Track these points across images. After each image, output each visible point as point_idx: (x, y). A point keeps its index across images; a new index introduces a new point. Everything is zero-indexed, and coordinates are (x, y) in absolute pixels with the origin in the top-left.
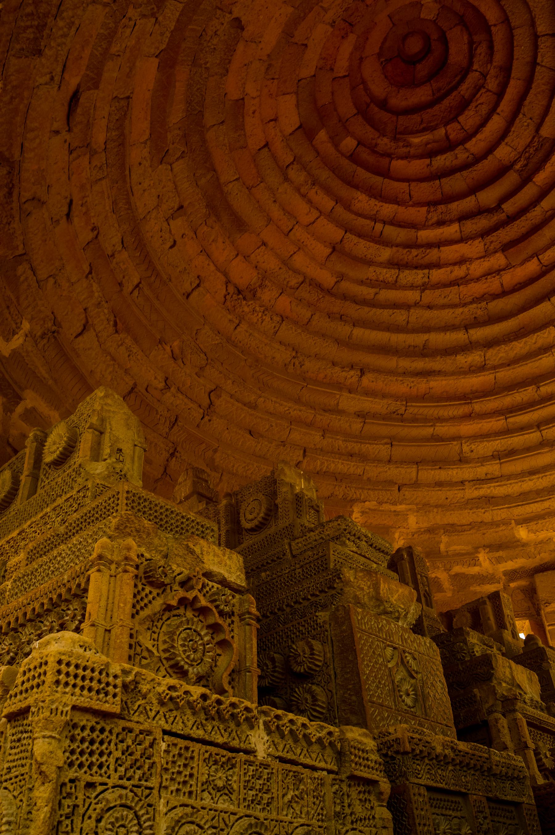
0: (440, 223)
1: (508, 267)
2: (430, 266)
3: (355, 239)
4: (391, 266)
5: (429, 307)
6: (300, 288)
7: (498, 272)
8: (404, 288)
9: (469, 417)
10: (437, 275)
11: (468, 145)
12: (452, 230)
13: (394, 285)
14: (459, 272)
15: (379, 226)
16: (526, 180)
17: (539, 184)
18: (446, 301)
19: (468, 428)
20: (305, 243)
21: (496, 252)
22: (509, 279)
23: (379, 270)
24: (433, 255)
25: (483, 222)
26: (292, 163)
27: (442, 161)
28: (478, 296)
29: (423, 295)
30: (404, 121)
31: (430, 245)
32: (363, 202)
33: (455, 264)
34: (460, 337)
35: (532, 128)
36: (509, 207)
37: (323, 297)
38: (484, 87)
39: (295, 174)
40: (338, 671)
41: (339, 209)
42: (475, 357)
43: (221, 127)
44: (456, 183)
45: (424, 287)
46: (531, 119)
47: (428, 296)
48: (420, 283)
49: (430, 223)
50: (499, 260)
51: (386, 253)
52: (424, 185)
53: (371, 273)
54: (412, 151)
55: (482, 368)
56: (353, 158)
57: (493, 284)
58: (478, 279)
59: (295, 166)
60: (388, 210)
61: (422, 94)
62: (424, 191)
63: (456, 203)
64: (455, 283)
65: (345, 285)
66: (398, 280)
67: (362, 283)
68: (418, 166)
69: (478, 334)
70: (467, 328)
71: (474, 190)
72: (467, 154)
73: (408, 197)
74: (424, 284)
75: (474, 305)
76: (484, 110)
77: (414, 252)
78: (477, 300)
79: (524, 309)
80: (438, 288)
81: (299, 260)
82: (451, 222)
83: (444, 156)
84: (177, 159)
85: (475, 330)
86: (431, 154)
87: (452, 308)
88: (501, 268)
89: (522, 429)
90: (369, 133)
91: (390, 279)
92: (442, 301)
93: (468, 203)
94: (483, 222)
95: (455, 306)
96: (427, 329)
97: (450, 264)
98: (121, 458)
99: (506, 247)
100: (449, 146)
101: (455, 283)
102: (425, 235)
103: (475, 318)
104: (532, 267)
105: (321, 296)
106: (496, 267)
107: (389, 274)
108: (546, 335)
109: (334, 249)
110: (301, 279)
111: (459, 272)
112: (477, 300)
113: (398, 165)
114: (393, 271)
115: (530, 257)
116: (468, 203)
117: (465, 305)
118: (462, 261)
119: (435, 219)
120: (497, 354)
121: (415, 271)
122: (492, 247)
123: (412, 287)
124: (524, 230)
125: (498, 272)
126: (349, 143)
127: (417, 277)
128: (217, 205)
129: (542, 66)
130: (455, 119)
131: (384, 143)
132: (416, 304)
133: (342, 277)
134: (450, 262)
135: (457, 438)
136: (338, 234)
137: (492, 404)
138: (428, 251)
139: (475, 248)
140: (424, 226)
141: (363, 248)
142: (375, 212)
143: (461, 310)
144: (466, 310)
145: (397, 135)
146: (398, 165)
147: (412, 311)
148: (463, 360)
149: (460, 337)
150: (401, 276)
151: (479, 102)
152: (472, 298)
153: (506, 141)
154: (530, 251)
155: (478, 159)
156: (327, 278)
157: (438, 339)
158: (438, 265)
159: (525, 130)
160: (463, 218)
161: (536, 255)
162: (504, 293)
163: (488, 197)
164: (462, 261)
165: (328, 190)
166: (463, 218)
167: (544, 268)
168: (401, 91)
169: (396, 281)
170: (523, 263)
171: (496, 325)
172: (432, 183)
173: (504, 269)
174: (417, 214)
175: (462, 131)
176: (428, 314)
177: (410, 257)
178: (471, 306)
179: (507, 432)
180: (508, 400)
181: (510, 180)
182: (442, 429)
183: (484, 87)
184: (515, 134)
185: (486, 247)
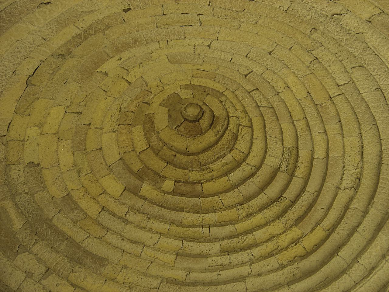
0: (249, 216)
2: (250, 247)
3: (191, 244)
4: (223, 254)
5: (259, 275)
6: (161, 287)
8: (236, 266)
10: (257, 252)
11: (248, 161)
12: (259, 218)
13: (229, 266)
14: (270, 246)
15: (206, 230)
16: (292, 175)
17: (301, 176)
18: (269, 268)
20: (155, 257)
21: (292, 226)
23: (214, 259)
24: (249, 239)
25: (275, 209)
26: (128, 212)
27: (235, 176)
28: (291, 259)
29: (252, 267)
30: (203, 157)
31: (246, 232)
32: (189, 217)
33: (266, 241)
35: (279, 143)
36: (289, 195)
37: (179, 288)
38: (241, 125)
39: (132, 217)
41: (174, 228)
43: (60, 215)
44: (249, 188)
45: (251, 262)
46: (276, 138)
47: (256, 268)
48: (247, 260)
49: (242, 217)
51: (216, 247)
52: (229, 194)
53: (210, 261)
54: (215, 174)
56: (175, 193)
57: (298, 250)
59: (131, 213)
60: (210, 217)
61: (210, 137)
62: (231, 198)
63: (254, 201)
64: (270, 255)
65: (194, 276)
66: (231, 261)
67: (205, 270)
68: (221, 183)
71: (262, 189)
72: (250, 167)
73: (221, 204)
74: (250, 260)
76: (248, 138)
77: (236, 240)
78: (292, 262)
79: (323, 263)
80: (261, 260)
81: (154, 270)
82: (256, 212)
83: (236, 172)
84: (34, 245)
85: (294, 285)
86: (227, 173)
87: (275, 272)
88: (299, 236)
90: (180, 173)
91: (226, 262)
92: (266, 268)
93: (262, 199)
94: (275, 209)
97: (264, 242)
100: (238, 164)
101: (270, 255)
102: (240, 227)
103: (294, 275)
104: (319, 233)
105: (178, 288)
106: (296, 237)
107: (224, 260)
108: (343, 281)
109: (177, 255)
110: (159, 281)
111: (270, 246)
112: (292, 262)
113: (208, 187)
114: (225, 257)
115: (315, 226)
116: (262, 199)
118: (272, 238)
119: (244, 214)
121: (240, 253)
122: (288, 224)
123: (243, 264)
124: (304, 209)
126: (168, 185)
127: (244, 256)
128: (79, 256)
129: (263, 107)
130: (233, 148)
131: (194, 176)
132: (249, 275)
133: (190, 271)
134: (264, 240)
136: (178, 243)
138: (245, 238)
139: (276, 227)
140: (238, 221)
141: (197, 248)
142: (201, 221)
143: (282, 272)
144: (285, 271)
145: (202, 167)
146: (208, 187)
147: (247, 280)
150: (232, 258)
151: (242, 134)
152: (287, 261)
153: (268, 154)
154: (313, 222)
155: (258, 168)
156: (180, 275)
158: (255, 245)
159: (276, 145)
160: (263, 208)
162: (308, 254)
163: (273, 191)
164: (272, 238)
165: (161, 219)
166: (263, 208)
167: (327, 231)
168: (195, 140)
169: (230, 263)
171: (308, 279)
172: (233, 191)
174: (232, 214)
175: (241, 153)
176: (259, 280)
177: (234, 244)
178: (287, 268)
181: (281, 179)
183: (241, 125)
184: (272, 149)
185: (284, 224)
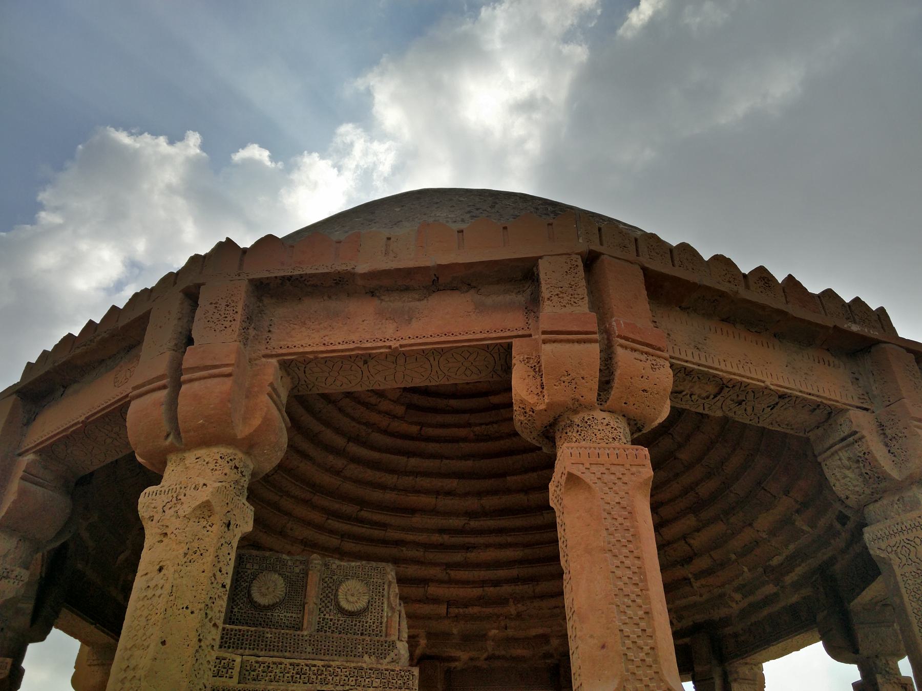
1: (401, 418)
7: (395, 417)
9: (306, 502)
19: (301, 511)
22: (396, 426)
34: (340, 441)
40: (251, 652)
42: (339, 463)
50: (400, 410)
55: (338, 473)
57: (384, 422)
58: (380, 412)
69: (354, 449)
70: (350, 439)
75: (364, 428)
79: (389, 451)
89: (332, 532)
95: (353, 419)
96: (327, 424)
98: (649, 631)
99: (410, 406)
104: (414, 429)
117: (359, 423)
120: (354, 470)
125: (395, 417)
135: (288, 514)
137: (326, 502)
148: (331, 460)
149: (340, 441)
157: (329, 435)
161: (422, 425)
162: (385, 432)
170: (411, 423)
173: (397, 418)
179: (320, 528)
180: (336, 506)
182: (287, 504)
